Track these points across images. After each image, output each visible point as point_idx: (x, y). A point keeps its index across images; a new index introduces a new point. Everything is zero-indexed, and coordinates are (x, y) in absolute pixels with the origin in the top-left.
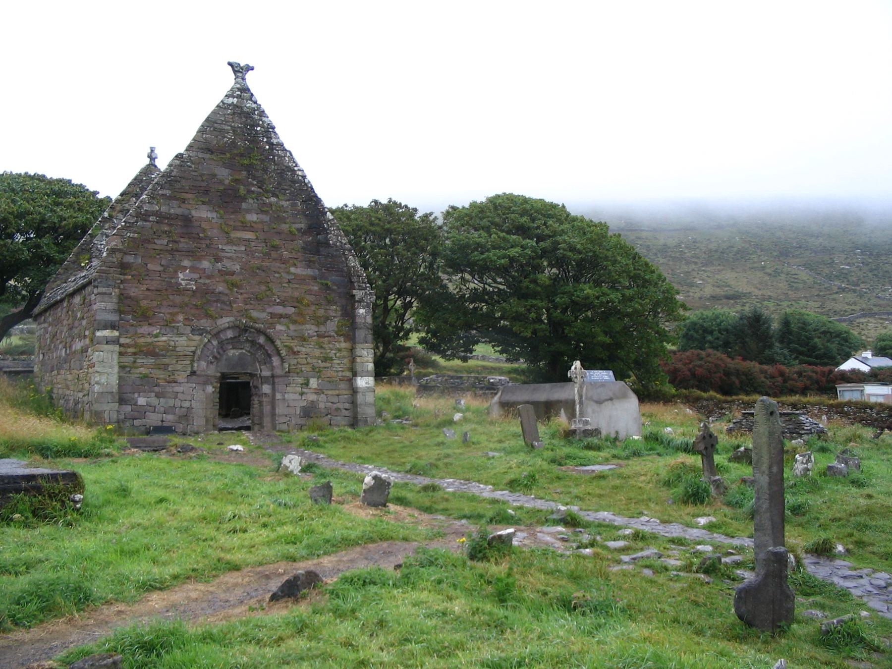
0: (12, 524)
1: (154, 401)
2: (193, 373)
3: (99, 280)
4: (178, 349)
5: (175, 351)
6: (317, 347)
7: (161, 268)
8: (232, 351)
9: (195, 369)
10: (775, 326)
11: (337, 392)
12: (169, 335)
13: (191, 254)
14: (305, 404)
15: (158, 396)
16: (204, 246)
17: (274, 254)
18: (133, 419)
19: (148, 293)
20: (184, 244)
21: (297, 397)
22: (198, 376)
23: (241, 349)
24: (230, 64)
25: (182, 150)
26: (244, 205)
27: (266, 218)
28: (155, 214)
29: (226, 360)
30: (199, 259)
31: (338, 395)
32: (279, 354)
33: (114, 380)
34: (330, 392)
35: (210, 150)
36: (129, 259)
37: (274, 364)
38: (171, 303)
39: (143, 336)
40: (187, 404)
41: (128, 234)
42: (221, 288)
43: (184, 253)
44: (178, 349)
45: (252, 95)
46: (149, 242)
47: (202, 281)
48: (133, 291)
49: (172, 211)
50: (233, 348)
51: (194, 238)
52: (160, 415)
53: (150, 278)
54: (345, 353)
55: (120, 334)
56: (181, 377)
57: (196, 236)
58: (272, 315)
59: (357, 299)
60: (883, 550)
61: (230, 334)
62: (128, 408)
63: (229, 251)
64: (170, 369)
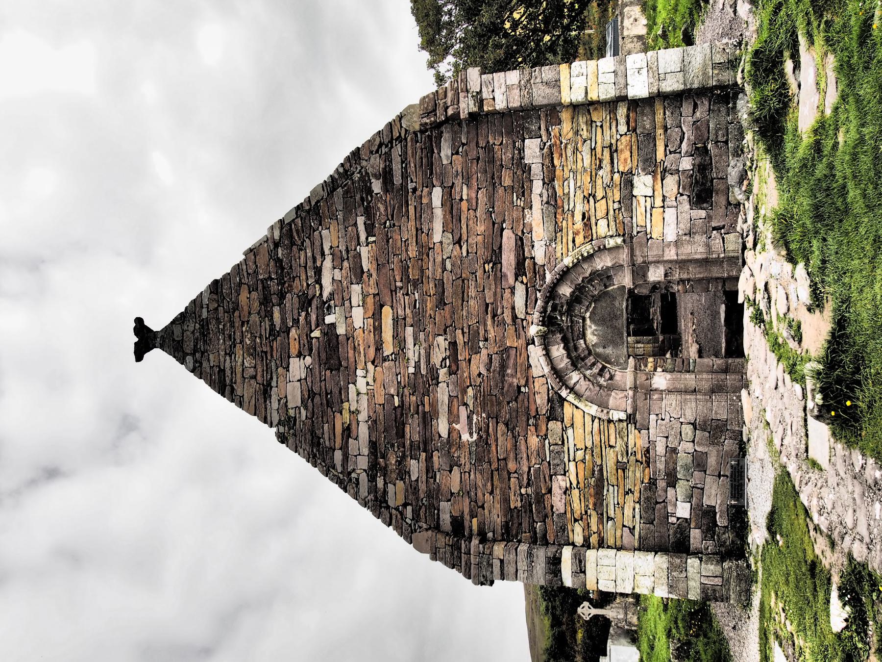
0: (743, 585)
2: (631, 419)
4: (589, 445)
6: (575, 261)
9: (623, 416)
11: (660, 131)
12: (566, 460)
13: (428, 419)
15: (672, 482)
16: (413, 398)
20: (413, 430)
21: (670, 214)
22: (635, 409)
23: (584, 319)
24: (139, 357)
26: (341, 330)
29: (604, 347)
31: (666, 129)
32: (590, 257)
37: (610, 265)
39: (568, 503)
40: (688, 430)
44: (589, 445)
48: (495, 516)
50: (584, 336)
52: (709, 479)
54: (582, 120)
55: (568, 544)
56: (636, 440)
58: (520, 270)
59: (476, 109)
61: (558, 351)
62: (695, 535)
64: (625, 460)
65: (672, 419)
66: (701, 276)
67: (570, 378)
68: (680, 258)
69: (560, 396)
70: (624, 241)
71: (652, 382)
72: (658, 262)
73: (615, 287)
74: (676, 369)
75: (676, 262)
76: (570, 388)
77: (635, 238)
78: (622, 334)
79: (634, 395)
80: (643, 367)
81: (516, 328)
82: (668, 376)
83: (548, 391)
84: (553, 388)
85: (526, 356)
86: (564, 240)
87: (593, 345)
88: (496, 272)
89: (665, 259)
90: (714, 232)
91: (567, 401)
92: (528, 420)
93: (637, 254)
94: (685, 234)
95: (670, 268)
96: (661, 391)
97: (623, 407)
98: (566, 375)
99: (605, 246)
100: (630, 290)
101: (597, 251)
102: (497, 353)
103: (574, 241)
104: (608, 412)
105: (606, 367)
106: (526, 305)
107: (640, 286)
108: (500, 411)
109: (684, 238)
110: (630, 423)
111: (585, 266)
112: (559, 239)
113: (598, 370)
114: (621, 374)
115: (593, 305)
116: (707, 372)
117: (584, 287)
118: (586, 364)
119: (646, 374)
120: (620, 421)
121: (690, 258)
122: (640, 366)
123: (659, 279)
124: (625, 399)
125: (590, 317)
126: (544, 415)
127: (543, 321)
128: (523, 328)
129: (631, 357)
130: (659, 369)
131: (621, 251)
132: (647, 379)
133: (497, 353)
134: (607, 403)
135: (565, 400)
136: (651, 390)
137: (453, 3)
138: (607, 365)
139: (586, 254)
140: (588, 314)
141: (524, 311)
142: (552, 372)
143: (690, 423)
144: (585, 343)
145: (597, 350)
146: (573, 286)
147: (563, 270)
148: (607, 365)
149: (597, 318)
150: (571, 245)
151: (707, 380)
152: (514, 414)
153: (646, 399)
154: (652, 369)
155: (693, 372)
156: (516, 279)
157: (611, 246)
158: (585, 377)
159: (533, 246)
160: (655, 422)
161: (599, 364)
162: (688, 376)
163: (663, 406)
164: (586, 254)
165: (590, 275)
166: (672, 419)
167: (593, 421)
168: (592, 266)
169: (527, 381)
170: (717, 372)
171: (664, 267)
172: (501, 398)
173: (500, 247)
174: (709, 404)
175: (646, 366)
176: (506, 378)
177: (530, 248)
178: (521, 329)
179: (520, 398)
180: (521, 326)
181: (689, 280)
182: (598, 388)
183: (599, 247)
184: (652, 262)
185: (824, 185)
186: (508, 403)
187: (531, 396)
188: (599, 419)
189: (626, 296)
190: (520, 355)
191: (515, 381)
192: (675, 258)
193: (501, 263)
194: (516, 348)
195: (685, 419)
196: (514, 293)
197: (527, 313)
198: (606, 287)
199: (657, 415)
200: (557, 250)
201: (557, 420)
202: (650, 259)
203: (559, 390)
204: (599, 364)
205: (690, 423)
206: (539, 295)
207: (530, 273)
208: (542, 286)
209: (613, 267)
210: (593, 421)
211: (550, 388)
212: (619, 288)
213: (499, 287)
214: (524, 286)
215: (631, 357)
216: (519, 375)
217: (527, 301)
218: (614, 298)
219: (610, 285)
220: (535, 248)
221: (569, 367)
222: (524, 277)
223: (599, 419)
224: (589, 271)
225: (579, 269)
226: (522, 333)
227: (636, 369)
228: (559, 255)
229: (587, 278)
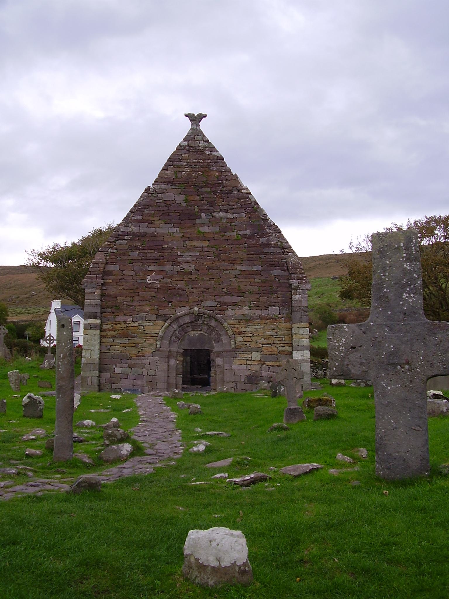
1: (128, 370)
3: (86, 284)
4: (146, 332)
5: (144, 333)
7: (134, 273)
8: (193, 333)
10: (213, 584)
11: (278, 364)
13: (157, 261)
14: (248, 373)
17: (223, 256)
18: (112, 383)
19: (125, 292)
24: (186, 115)
25: (150, 183)
26: (198, 221)
27: (217, 229)
28: (128, 233)
30: (163, 264)
33: (96, 356)
34: (270, 364)
35: (171, 182)
36: (111, 268)
38: (141, 298)
41: (110, 250)
42: (181, 284)
43: (150, 261)
44: (146, 332)
45: (204, 136)
46: (124, 254)
47: (164, 280)
48: (112, 290)
49: (142, 231)
51: (159, 249)
53: (125, 281)
57: (161, 247)
59: (293, 287)
60: (316, 301)
63: (186, 256)
66: (217, 380)
68: (225, 371)
69: (167, 320)
80: (179, 355)
103: (234, 327)
115: (207, 335)
127: (200, 313)
130: (178, 362)
140: (203, 332)
156: (219, 302)
158: (175, 331)
186: (164, 297)
192: (225, 369)
201: (157, 318)
212: (214, 346)
226: (195, 304)
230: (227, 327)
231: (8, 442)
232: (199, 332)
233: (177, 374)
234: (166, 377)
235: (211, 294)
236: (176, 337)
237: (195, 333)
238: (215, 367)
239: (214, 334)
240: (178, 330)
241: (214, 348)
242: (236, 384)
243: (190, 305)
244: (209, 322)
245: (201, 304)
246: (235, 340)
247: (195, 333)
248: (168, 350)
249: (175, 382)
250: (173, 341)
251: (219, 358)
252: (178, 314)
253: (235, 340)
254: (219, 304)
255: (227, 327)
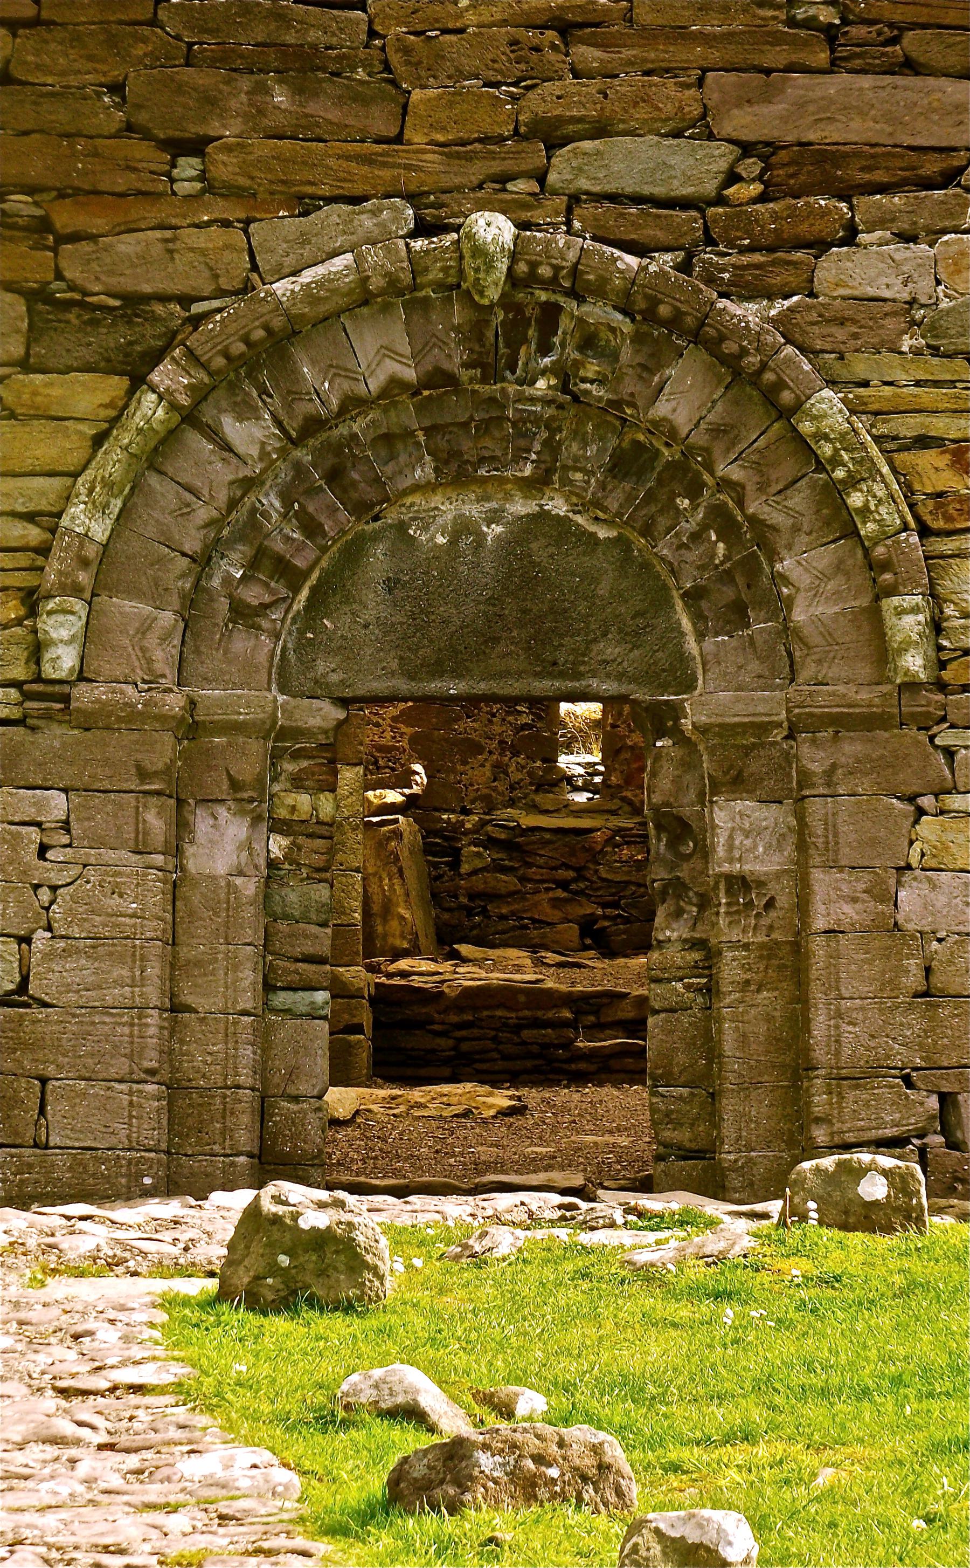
29: (391, 584)
37: (799, 615)
65: (45, 895)
66: (729, 1046)
67: (245, 411)
68: (818, 947)
69: (155, 358)
70: (911, 686)
71: (222, 812)
72: (802, 846)
73: (692, 646)
74: (283, 926)
75: (801, 932)
76: (196, 404)
77: (923, 737)
78: (457, 674)
79: (162, 718)
80: (290, 767)
81: (501, 139)
82: (249, 887)
83: (186, 300)
84: (196, 321)
85: (358, 189)
86: (927, 396)
87: (402, 527)
88: (794, 42)
89: (818, 876)
90: (933, 1103)
91: (131, 392)
92: (30, 190)
93: (848, 748)
94: (928, 970)
95: (770, 904)
96: (178, 852)
97: (105, 665)
98: (263, 392)
99: (891, 591)
100: (676, 711)
101: (867, 552)
102: (372, 34)
103: (923, 442)
104: (76, 591)
105: (296, 590)
106: (613, 198)
107: (690, 763)
108: (77, 39)
109: (913, 965)
110: (28, 696)
111: (799, 500)
112: (936, 368)
113: (278, 546)
114: (262, 657)
115: (603, 533)
116: (262, 1069)
117: (694, 490)
118: (314, 491)
119: (259, 782)
120: (37, 650)
121: (817, 993)
122: (296, 755)
123: (721, 852)
124: (140, 674)
125: (543, 515)
126: (59, 276)
127: (532, 279)
128: (503, 179)
129: (341, 714)
130: (277, 845)
131: (865, 671)
132: (235, 785)
133: (372, 34)
134: (113, 591)
135: (138, 381)
136: (181, 802)
137: (428, 789)
138: (305, 593)
139: (856, 500)
140: (558, 506)
141: (584, 184)
142: (278, 323)
143: (25, 980)
144: (417, 488)
145: (380, 549)
146: (699, 439)
147: (780, 385)
148: (305, 593)
149: (539, 550)
150: (908, 426)
151: (229, 1062)
152: (60, 116)
153: (143, 774)
154: (283, 813)
155: (268, 1007)
156: (746, 148)
157: (890, 619)
158: (249, 484)
159: (908, 238)
160: (30, 813)
161: (311, 553)
162: (249, 977)
163: (110, 855)
164: (856, 500)
165: (753, 520)
166: (45, 895)
167: (30, 517)
168: (796, 529)
169: (233, 192)
170: (263, 1112)
171: (778, 875)
172: (140, 50)
173: (910, 66)
174: (120, 1066)
175: (297, 783)
176: (245, 83)
177: (903, 225)
178: (496, 167)
179: (141, 151)
180: (509, 166)
181: (710, 990)
182: (192, 544)
183: (886, 566)
184: (801, 817)
185: (499, 1363)
186: (116, 88)
187: (154, 214)
188: (44, 550)
189: (642, 695)
190: (368, 160)
191: (229, 131)
192: (820, 923)
193: (834, 66)
194: (398, 139)
195: (49, 956)
196: (677, 134)
197: (575, 199)
198: (693, 597)
199: (66, 826)
200: (886, 357)
201: (33, 334)
202: (816, 809)
203: (191, 354)
204: (311, 553)
205: (25, 980)
206: (667, 259)
207: (775, 217)
208: (710, 280)
209: (787, 631)
210: (30, 517)
211: (197, 308)
212: (682, 658)
213: (715, 56)
214: (710, 187)
215: (341, 714)
216: (263, 148)
217: (637, 199)
218: (633, 637)
219: (698, 617)
220: (898, 251)
221: (303, 408)
222: (756, 189)
223: (44, 550)
224: (776, 518)
225: (787, 468)
226: (477, 171)
227: (284, 734)
228: (860, 366)
229: (740, 503)
230: (848, 440)
231: (649, 430)
232: (520, 507)
233: (269, 987)
234: (153, 1019)
235: (654, 55)
236: (252, 565)
237: (473, 510)
238: (704, 903)
239: (689, 526)
240: (284, 473)
241: (689, 686)
242: (945, 1098)
243: (413, 181)
244: (629, 386)
245: (541, 179)
246: (934, 596)
247: (473, 510)
248: (174, 702)
249: (245, 1079)
250: (223, 605)
251: (747, 805)
252: (281, 287)
253: (934, 596)
254: (751, 167)
255: (848, 440)
